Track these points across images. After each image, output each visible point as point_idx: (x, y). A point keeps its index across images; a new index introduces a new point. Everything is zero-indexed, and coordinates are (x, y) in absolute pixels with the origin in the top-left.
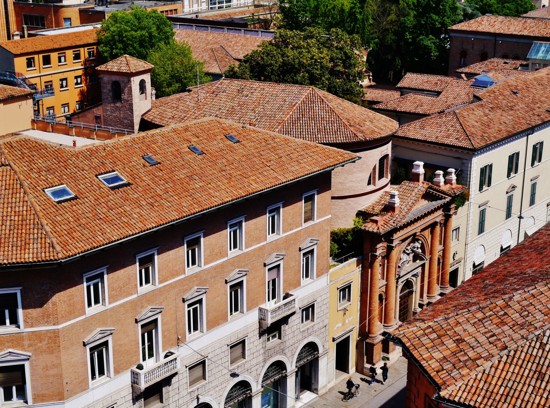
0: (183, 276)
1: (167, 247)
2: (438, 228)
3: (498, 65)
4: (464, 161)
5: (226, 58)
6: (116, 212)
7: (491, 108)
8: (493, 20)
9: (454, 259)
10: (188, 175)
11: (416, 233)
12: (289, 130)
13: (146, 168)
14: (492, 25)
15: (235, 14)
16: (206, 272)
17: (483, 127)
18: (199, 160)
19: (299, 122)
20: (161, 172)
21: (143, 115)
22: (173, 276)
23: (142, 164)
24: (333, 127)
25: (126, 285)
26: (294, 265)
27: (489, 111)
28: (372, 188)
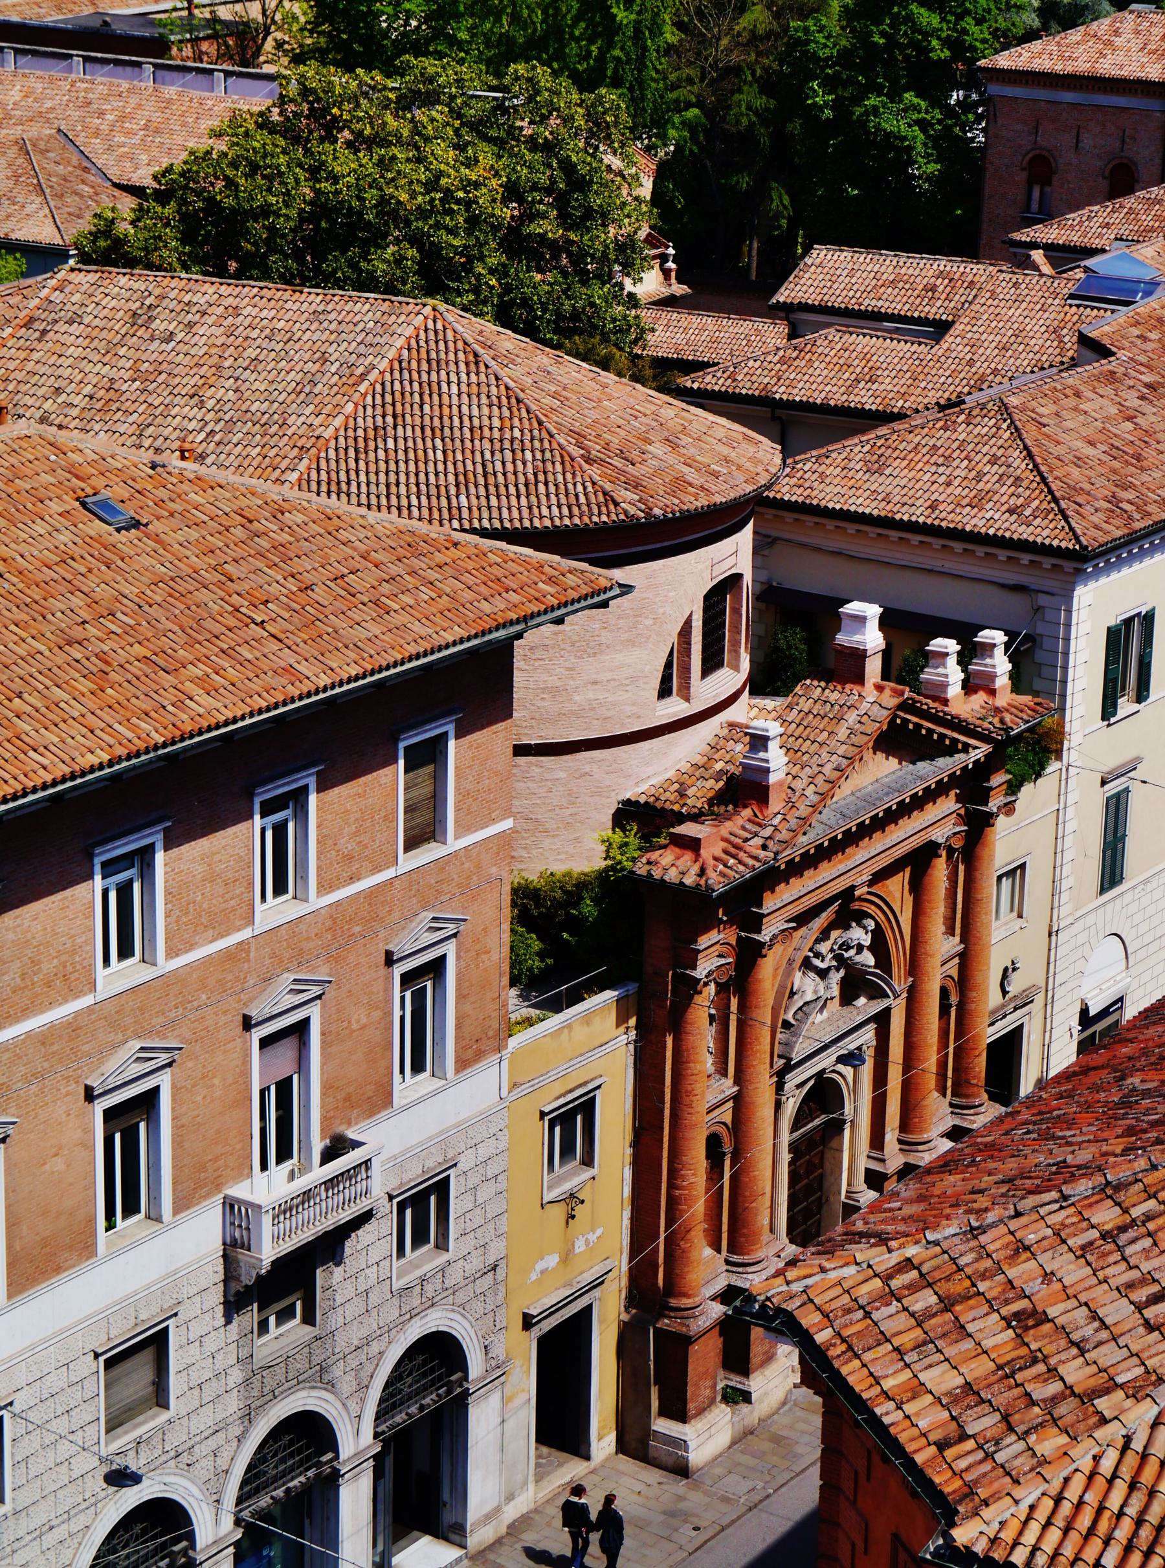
4: (1043, 600)
7: (1148, 386)
9: (1005, 993)
11: (852, 888)
17: (1116, 464)
19: (381, 445)
26: (364, 1020)
27: (1142, 398)
28: (675, 708)
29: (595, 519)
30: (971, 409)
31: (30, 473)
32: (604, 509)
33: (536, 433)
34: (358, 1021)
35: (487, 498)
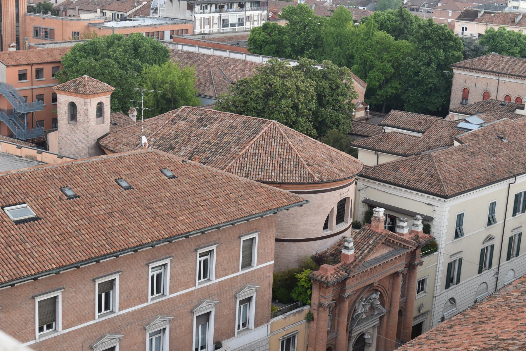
0: (92, 322)
1: (74, 289)
2: (401, 278)
3: (493, 107)
4: (436, 208)
5: (224, 82)
6: (14, 249)
7: (472, 152)
8: (498, 60)
9: (419, 312)
10: (108, 212)
11: (373, 283)
12: (243, 165)
13: (62, 201)
14: (496, 65)
15: (243, 37)
16: (121, 318)
17: (460, 173)
18: (125, 195)
19: (254, 157)
20: (78, 206)
21: (99, 139)
22: (80, 322)
23: (58, 197)
24: (289, 165)
25: (22, 330)
26: (228, 313)
27: (469, 156)
28: (328, 232)
29: (307, 181)
30: (422, 156)
31: (149, 162)
32: (310, 179)
33: (295, 157)
34: (226, 313)
35: (279, 173)
